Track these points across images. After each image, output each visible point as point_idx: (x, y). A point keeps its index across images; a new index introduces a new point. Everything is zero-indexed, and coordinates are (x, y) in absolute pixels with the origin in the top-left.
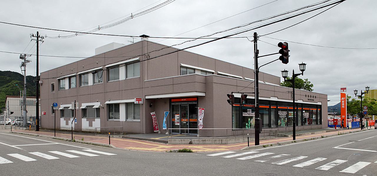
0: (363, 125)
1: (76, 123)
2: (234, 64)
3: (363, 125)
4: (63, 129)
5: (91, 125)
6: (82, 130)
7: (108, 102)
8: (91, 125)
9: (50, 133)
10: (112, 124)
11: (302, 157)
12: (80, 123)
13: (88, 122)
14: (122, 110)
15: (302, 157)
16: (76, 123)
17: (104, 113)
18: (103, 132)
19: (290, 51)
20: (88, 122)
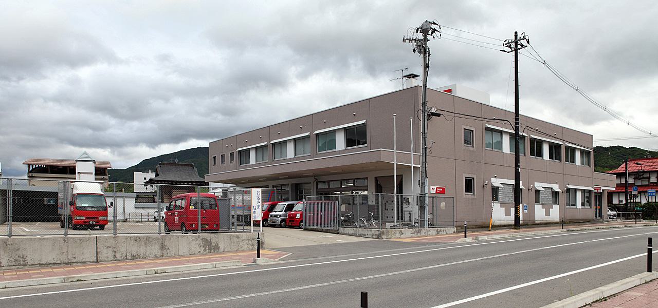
0: (174, 192)
1: (526, 211)
2: (551, 122)
3: (174, 192)
4: (498, 223)
5: (548, 214)
6: (536, 222)
7: (316, 132)
8: (548, 214)
9: (574, 225)
10: (571, 213)
11: (152, 266)
12: (533, 211)
13: (504, 208)
14: (253, 154)
15: (152, 266)
16: (526, 211)
17: (563, 198)
18: (562, 223)
19: (429, 40)
20: (504, 208)
